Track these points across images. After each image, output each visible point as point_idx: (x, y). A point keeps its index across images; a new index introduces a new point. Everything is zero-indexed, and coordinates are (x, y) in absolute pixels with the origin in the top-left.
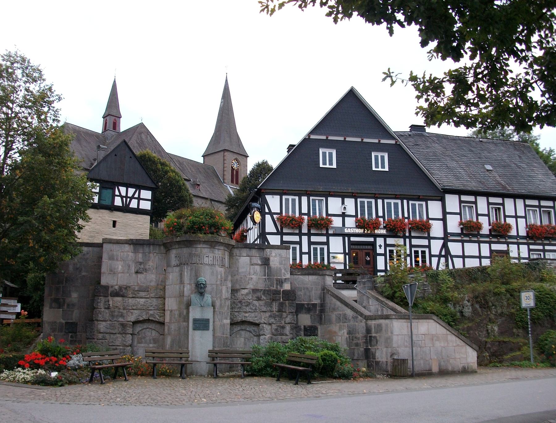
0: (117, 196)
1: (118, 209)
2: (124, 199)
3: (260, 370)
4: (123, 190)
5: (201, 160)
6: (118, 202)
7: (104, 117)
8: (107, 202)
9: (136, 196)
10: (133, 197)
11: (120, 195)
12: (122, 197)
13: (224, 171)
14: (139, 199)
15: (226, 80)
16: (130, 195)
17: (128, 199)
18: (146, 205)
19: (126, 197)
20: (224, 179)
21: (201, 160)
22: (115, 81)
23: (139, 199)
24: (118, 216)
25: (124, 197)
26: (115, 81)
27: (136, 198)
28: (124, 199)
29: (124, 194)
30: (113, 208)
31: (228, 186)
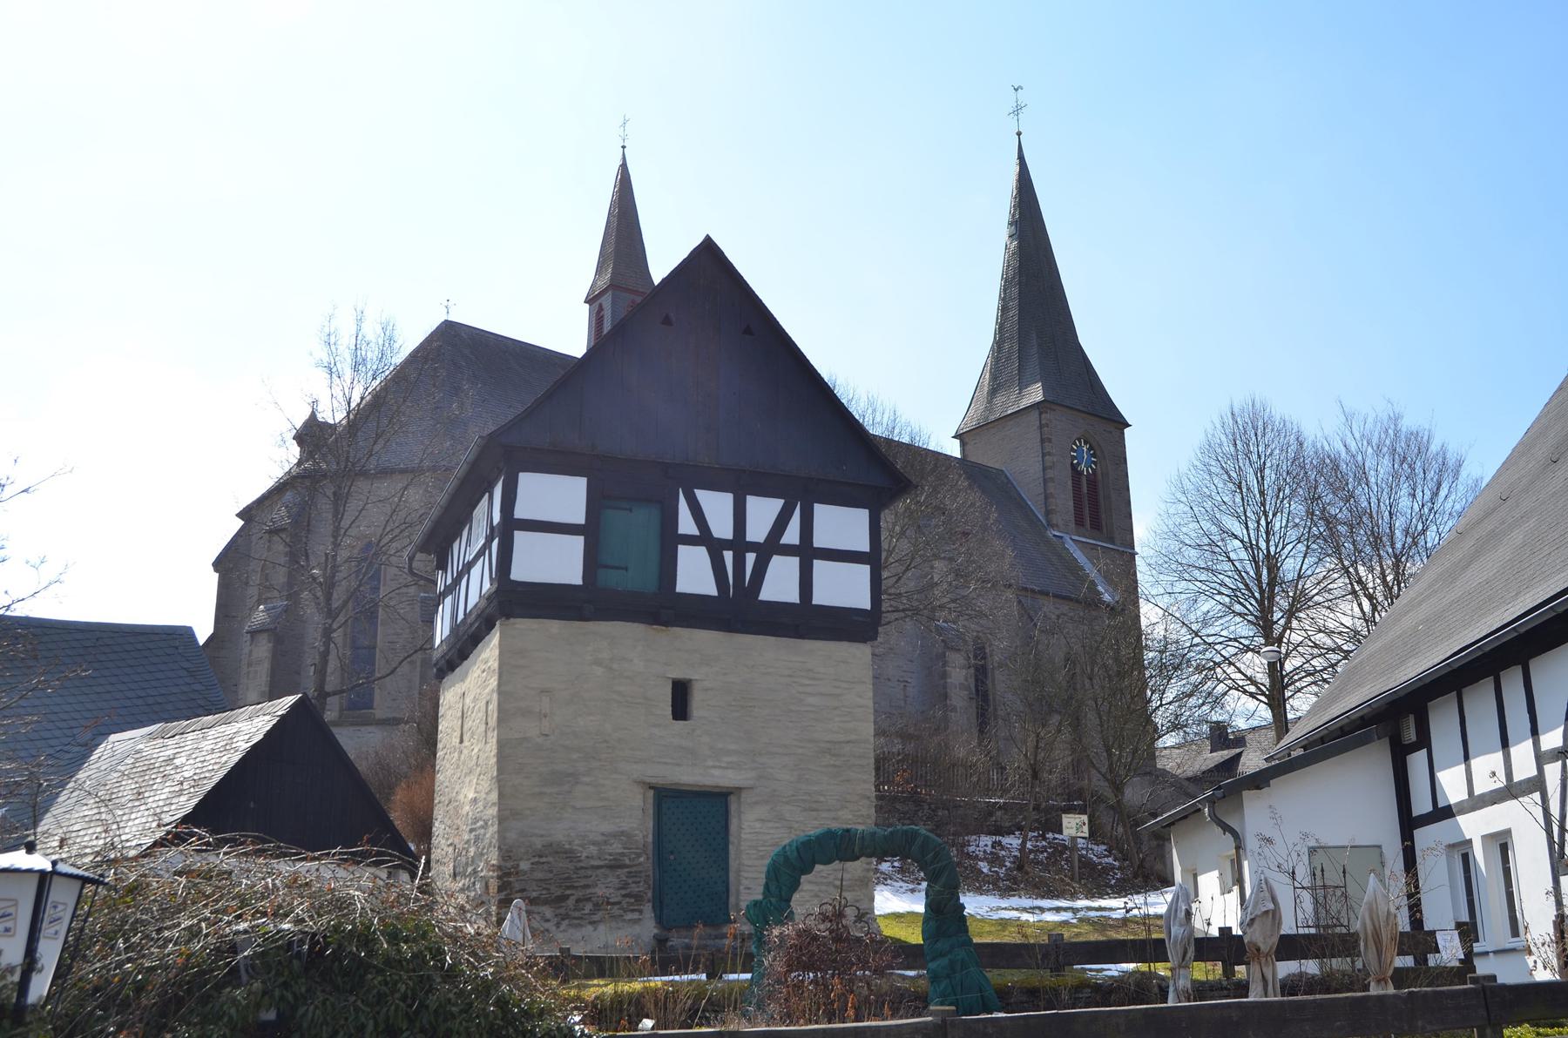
0: (689, 540)
1: (694, 613)
2: (728, 556)
3: (302, 523)
4: (718, 507)
5: (953, 449)
6: (694, 574)
7: (590, 300)
8: (638, 578)
9: (792, 536)
10: (772, 546)
11: (704, 537)
12: (715, 547)
13: (1045, 481)
14: (807, 553)
15: (1021, 158)
16: (757, 530)
17: (751, 558)
18: (844, 587)
19: (739, 543)
20: (1048, 513)
21: (953, 449)
22: (624, 167)
23: (807, 553)
24: (702, 653)
25: (724, 544)
26: (624, 167)
27: (788, 550)
28: (728, 556)
29: (722, 527)
30: (667, 609)
31: (1067, 537)
